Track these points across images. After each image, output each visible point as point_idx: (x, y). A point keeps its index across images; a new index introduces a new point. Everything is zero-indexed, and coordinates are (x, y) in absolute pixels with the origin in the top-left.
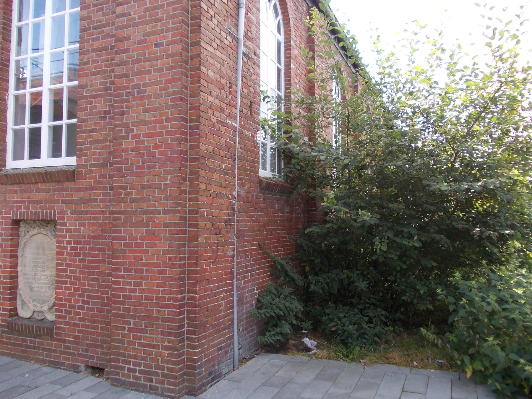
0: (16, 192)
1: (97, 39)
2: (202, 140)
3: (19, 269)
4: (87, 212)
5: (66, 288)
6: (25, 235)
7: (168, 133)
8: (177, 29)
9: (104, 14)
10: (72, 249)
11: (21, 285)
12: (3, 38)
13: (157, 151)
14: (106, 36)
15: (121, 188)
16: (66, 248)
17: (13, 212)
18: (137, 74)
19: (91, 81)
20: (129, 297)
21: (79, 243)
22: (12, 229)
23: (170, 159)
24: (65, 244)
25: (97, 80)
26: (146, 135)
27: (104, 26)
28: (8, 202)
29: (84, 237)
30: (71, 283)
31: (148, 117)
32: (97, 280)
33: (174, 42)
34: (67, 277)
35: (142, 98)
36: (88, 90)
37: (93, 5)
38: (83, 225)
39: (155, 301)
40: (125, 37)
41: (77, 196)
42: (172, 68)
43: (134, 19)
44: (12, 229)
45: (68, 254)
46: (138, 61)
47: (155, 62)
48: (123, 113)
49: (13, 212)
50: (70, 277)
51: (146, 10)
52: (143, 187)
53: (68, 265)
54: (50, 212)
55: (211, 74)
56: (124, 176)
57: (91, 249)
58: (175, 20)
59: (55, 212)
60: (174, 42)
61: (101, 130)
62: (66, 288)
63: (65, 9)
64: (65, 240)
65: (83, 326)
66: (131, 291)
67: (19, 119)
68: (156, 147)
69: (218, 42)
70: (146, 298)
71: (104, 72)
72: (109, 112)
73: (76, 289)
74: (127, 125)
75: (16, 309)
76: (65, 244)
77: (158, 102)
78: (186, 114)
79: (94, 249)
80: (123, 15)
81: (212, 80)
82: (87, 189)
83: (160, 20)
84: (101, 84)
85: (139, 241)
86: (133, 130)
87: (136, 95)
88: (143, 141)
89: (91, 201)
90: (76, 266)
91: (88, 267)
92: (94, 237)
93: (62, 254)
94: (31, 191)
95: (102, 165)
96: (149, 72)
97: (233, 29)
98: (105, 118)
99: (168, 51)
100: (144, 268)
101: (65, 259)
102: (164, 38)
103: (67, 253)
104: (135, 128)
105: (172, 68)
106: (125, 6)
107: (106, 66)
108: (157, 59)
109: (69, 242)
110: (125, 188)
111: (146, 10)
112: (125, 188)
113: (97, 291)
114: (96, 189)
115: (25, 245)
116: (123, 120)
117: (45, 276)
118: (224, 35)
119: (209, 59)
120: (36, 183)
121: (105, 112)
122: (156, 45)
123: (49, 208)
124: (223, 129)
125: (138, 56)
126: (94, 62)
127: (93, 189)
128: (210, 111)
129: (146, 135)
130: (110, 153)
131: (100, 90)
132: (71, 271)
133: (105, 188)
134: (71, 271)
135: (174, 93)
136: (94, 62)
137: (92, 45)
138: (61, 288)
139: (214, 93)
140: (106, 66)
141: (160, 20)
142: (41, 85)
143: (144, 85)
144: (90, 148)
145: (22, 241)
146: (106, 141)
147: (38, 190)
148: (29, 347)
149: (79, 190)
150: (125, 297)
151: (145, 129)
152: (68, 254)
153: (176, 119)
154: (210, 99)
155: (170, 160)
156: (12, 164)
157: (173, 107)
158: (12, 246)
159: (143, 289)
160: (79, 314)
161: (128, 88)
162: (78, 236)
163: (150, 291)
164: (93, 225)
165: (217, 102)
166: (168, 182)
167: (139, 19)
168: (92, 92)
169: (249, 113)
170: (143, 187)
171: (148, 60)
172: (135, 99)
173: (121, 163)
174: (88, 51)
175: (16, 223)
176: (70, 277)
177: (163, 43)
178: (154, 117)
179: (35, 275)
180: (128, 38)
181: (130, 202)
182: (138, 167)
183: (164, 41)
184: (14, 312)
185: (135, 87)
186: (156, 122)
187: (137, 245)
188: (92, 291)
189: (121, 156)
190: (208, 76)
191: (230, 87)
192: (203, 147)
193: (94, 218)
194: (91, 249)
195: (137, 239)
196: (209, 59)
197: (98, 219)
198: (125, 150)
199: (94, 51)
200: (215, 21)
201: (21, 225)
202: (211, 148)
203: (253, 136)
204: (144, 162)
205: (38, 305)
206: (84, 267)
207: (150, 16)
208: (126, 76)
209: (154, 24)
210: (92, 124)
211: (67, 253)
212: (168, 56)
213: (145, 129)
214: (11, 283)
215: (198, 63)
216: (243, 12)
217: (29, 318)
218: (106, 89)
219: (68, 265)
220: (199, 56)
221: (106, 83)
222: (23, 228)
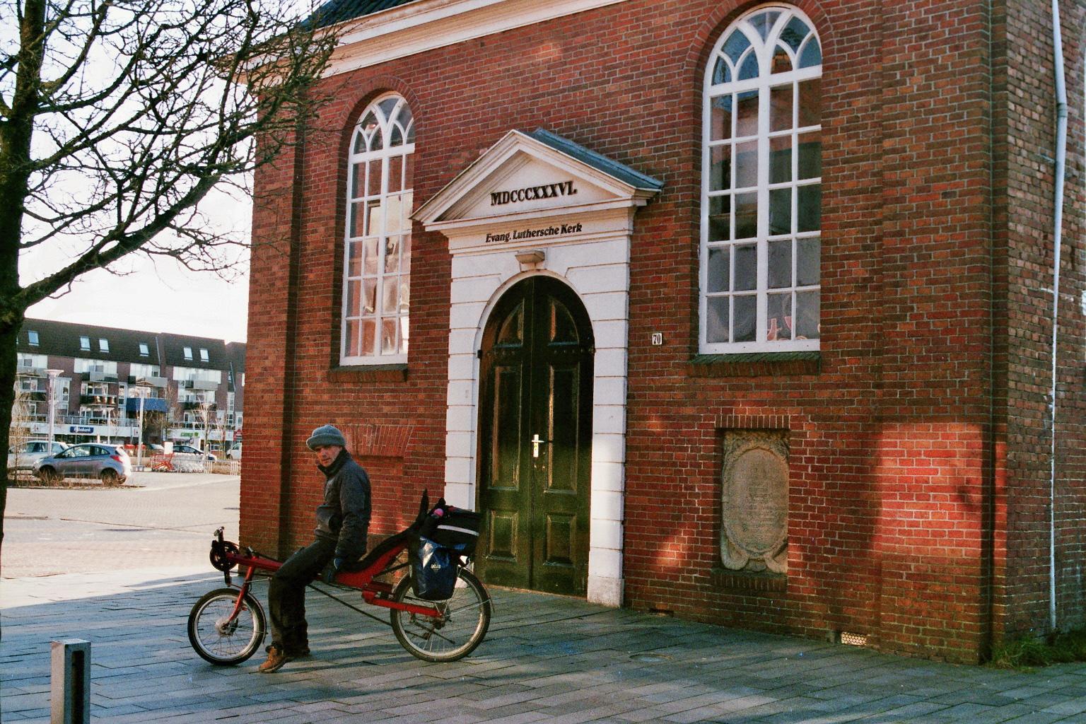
0: (723, 388)
1: (850, 177)
2: (1011, 322)
3: (725, 499)
4: (839, 418)
5: (806, 525)
6: (734, 449)
7: (964, 314)
8: (975, 174)
9: (860, 143)
10: (814, 469)
11: (727, 522)
12: (694, 166)
13: (948, 337)
14: (864, 174)
15: (895, 385)
16: (806, 468)
17: (719, 417)
18: (915, 233)
19: (842, 235)
20: (909, 533)
21: (826, 461)
22: (715, 442)
23: (966, 348)
24: (804, 463)
25: (852, 234)
26: (934, 316)
27: (861, 159)
28: (709, 403)
29: (834, 453)
30: (813, 517)
31: (933, 291)
32: (854, 512)
33: (971, 193)
34: (808, 508)
35: (925, 265)
36: (837, 248)
37: (842, 128)
38: (832, 436)
39: (947, 538)
40: (897, 182)
41: (825, 395)
42: (969, 227)
43: (911, 158)
44: (715, 442)
45: (808, 476)
46: (919, 214)
47: (943, 218)
48: (896, 285)
49: (719, 417)
50: (812, 509)
51: (929, 146)
52: (928, 384)
53: (808, 492)
54: (779, 418)
55: (1020, 229)
56: (900, 370)
57: (843, 470)
58: (972, 162)
59: (786, 418)
60: (971, 193)
61: (858, 305)
62: (806, 525)
63: (790, 127)
64: (803, 456)
65: (832, 577)
66: (911, 524)
67: (720, 281)
68: (946, 331)
69: (1028, 179)
70: (935, 534)
71: (862, 224)
72: (870, 280)
73: (820, 526)
74: (903, 301)
75: (720, 559)
76: (804, 463)
77: (951, 271)
78: (988, 288)
79: (850, 470)
80: (894, 151)
81: (1021, 236)
82: (838, 386)
83: (951, 161)
84: (857, 240)
85: (923, 457)
86: (912, 309)
87: (916, 260)
88: (928, 324)
89: (845, 402)
90: (821, 493)
91: (838, 494)
92: (849, 453)
93: (800, 476)
94: (748, 388)
95: (861, 353)
96: (936, 231)
97: (1048, 152)
98: (865, 288)
99: (963, 202)
100: (931, 494)
101: (805, 484)
102: (957, 186)
103: (807, 475)
104: (915, 305)
105: (969, 227)
106: (897, 139)
107: (864, 215)
108: (948, 213)
109: (810, 460)
110: (902, 386)
111: (929, 146)
112: (902, 386)
113: (855, 528)
114: (852, 386)
115: (733, 467)
116: (896, 294)
117: (768, 508)
118: (1035, 166)
119: (1019, 210)
120: (755, 376)
121: (864, 280)
122: (945, 195)
123: (777, 412)
124: (1035, 301)
125: (917, 208)
126: (846, 209)
127: (847, 386)
128: (1020, 281)
129: (934, 316)
130: (872, 337)
131: (855, 248)
132: (814, 501)
133: (866, 386)
134: (814, 501)
135: (973, 260)
136: (846, 209)
137: (842, 185)
138: (797, 524)
139: (1024, 255)
140: (864, 215)
141: (951, 161)
142: (754, 234)
143: (927, 248)
144: (842, 329)
145: (729, 459)
146: (866, 319)
147: (758, 387)
148: (748, 609)
149: (827, 386)
150: (901, 532)
151: (931, 307)
152: (808, 476)
153: (976, 295)
154: (1020, 263)
155: (967, 350)
156: (708, 348)
157: (970, 279)
158: (715, 465)
159: (930, 522)
160: (827, 559)
161: (903, 250)
162: (825, 452)
163: (942, 525)
164: (849, 435)
165: (1028, 265)
166: (966, 379)
167: (918, 157)
168: (844, 250)
169: (1070, 265)
170: (928, 384)
171: (934, 214)
172: (914, 266)
173: (895, 351)
174: (835, 193)
175: (721, 432)
176: (812, 509)
177: (955, 193)
178: (944, 291)
179: (751, 507)
180: (902, 183)
181: (909, 404)
182: (919, 359)
183: (957, 190)
184: (718, 559)
185: (912, 250)
186: (947, 298)
187: (920, 462)
188: (846, 528)
189: (895, 343)
190: (1017, 233)
191: (1045, 237)
192: (1012, 332)
193: (849, 427)
194: (843, 470)
195: (919, 454)
196: (1019, 210)
197: (856, 427)
198: (902, 334)
199: (844, 193)
200: (1024, 153)
201: (728, 437)
202: (1021, 332)
203: (1077, 301)
204: (928, 351)
205: (755, 550)
206: (834, 495)
207: (934, 155)
208: (900, 234)
209: (941, 166)
210: (844, 296)
211: (807, 475)
212: (964, 210)
213: (931, 307)
214: (714, 519)
215: (1004, 219)
216: (1063, 124)
217: (742, 569)
218: (866, 248)
219: (808, 492)
220: (1005, 208)
221: (866, 238)
222: (729, 441)
